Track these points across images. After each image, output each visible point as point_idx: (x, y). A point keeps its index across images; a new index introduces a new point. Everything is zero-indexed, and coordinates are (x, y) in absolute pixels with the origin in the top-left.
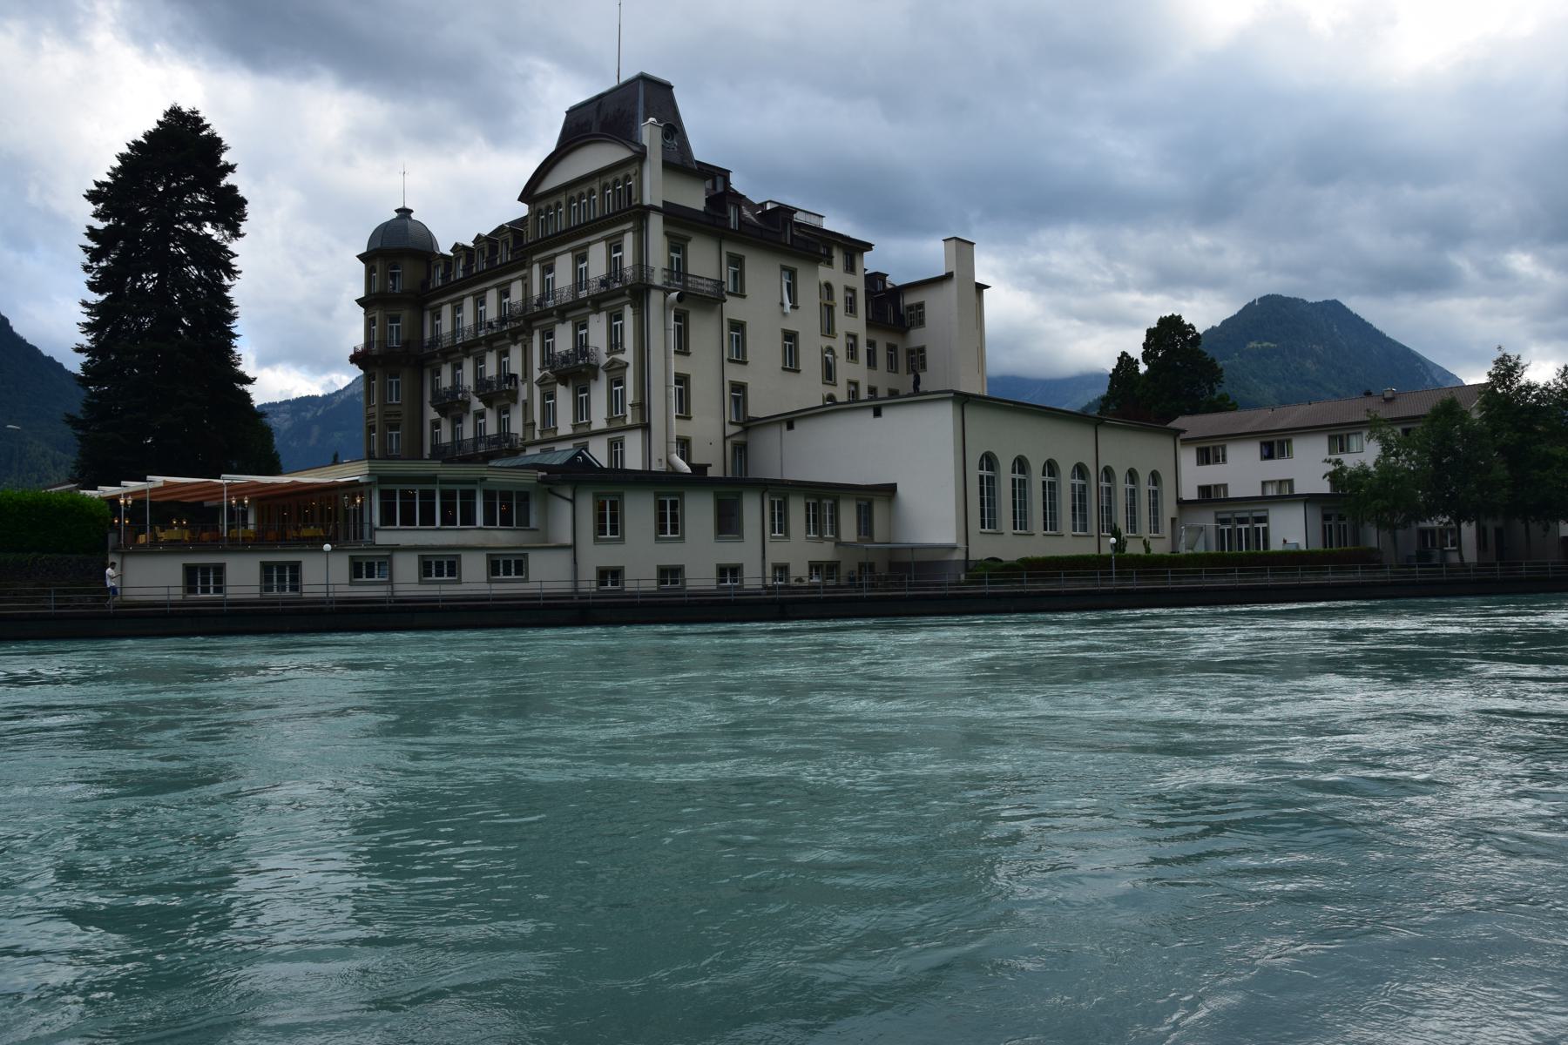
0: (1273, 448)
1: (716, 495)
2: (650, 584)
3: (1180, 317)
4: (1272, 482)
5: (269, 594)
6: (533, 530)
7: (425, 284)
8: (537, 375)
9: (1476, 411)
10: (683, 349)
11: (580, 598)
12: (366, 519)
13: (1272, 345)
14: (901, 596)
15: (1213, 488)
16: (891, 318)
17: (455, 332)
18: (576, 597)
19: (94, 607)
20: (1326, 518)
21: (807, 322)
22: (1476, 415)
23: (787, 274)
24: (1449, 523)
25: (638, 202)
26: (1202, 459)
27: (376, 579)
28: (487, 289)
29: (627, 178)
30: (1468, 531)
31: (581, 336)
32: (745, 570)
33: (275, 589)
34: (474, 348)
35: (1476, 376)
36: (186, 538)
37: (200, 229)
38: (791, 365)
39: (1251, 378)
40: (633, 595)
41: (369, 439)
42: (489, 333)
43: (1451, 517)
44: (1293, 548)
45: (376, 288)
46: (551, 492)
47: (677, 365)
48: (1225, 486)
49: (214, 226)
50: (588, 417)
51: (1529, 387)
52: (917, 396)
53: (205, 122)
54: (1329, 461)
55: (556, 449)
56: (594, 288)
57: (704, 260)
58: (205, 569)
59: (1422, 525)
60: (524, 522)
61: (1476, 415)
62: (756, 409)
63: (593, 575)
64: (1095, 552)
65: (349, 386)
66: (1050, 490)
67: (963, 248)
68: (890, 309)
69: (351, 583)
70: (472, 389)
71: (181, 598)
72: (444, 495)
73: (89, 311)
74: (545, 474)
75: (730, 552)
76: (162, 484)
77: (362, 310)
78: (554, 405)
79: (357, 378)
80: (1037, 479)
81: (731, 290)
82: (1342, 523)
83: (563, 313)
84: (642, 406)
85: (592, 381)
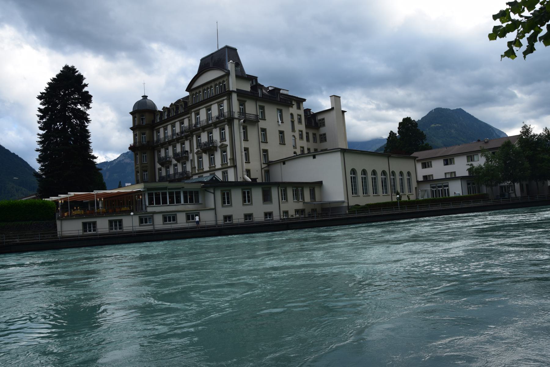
0: (448, 161)
1: (262, 188)
2: (242, 221)
3: (410, 118)
4: (448, 173)
5: (112, 231)
6: (200, 204)
7: (153, 121)
8: (195, 151)
9: (517, 145)
10: (246, 139)
11: (218, 226)
12: (143, 203)
13: (439, 125)
14: (328, 219)
15: (428, 176)
16: (313, 124)
17: (165, 137)
18: (217, 226)
19: (52, 239)
20: (468, 184)
21: (286, 127)
22: (517, 146)
23: (279, 111)
24: (511, 183)
25: (228, 89)
26: (424, 166)
27: (148, 224)
28: (175, 122)
29: (224, 81)
30: (517, 186)
31: (210, 136)
32: (254, 214)
33: (114, 229)
34: (172, 142)
35: (515, 132)
36: (83, 213)
37: (76, 106)
38: (282, 142)
39: (433, 137)
40: (237, 224)
41: (137, 176)
42: (178, 137)
43: (511, 181)
44: (458, 195)
45: (137, 124)
46: (206, 190)
47: (244, 144)
48: (432, 175)
49: (81, 105)
50: (214, 164)
51: (534, 135)
52: (325, 151)
53: (77, 70)
54: (468, 165)
55: (204, 176)
56: (214, 120)
57: (251, 108)
58: (90, 223)
59: (502, 184)
60: (197, 201)
61: (517, 146)
62: (272, 158)
63: (222, 218)
64: (391, 201)
65: (118, 158)
66: (374, 180)
67: (336, 99)
68: (313, 121)
69: (140, 226)
70: (172, 157)
71: (82, 234)
72: (170, 194)
73: (40, 137)
74: (203, 184)
75: (268, 208)
76: (73, 195)
77: (132, 131)
78: (202, 160)
79: (121, 155)
80: (370, 176)
81: (261, 118)
82: (474, 186)
83: (203, 129)
84: (233, 159)
85: (215, 152)
